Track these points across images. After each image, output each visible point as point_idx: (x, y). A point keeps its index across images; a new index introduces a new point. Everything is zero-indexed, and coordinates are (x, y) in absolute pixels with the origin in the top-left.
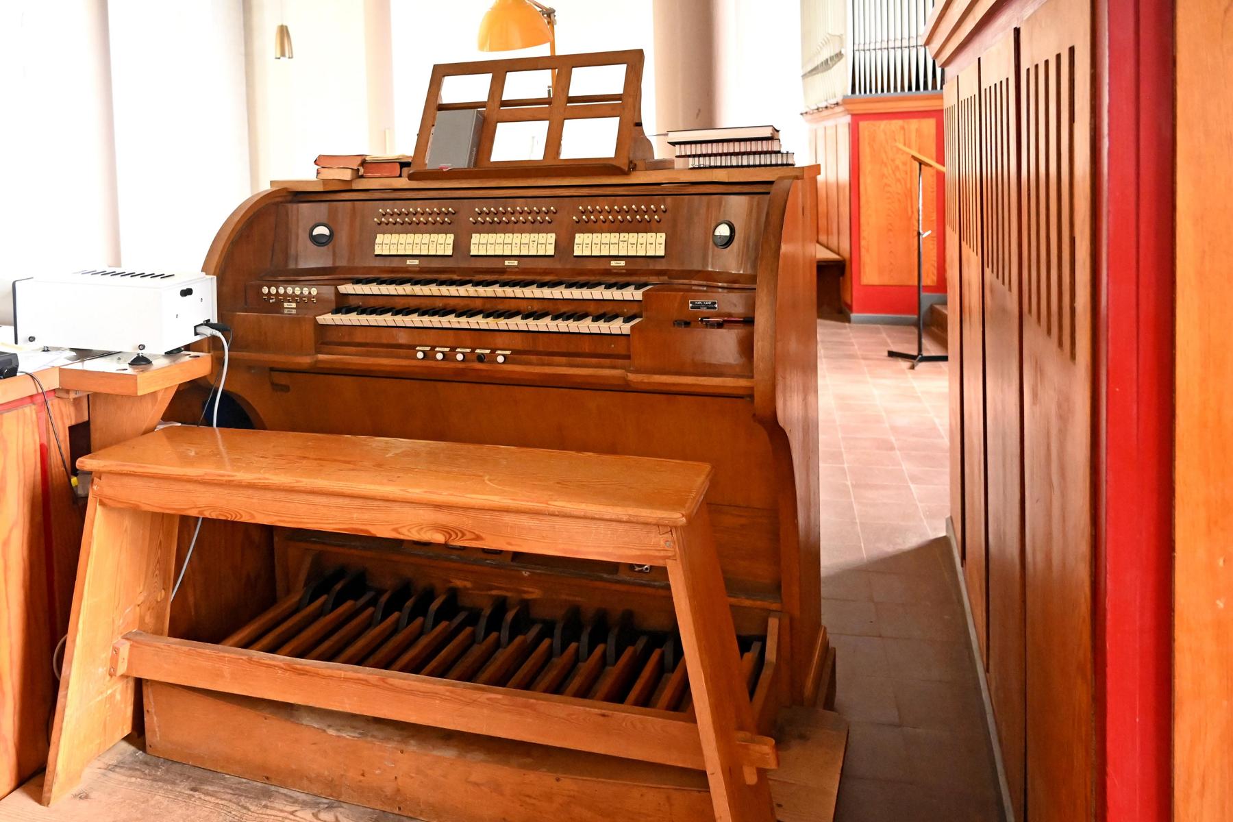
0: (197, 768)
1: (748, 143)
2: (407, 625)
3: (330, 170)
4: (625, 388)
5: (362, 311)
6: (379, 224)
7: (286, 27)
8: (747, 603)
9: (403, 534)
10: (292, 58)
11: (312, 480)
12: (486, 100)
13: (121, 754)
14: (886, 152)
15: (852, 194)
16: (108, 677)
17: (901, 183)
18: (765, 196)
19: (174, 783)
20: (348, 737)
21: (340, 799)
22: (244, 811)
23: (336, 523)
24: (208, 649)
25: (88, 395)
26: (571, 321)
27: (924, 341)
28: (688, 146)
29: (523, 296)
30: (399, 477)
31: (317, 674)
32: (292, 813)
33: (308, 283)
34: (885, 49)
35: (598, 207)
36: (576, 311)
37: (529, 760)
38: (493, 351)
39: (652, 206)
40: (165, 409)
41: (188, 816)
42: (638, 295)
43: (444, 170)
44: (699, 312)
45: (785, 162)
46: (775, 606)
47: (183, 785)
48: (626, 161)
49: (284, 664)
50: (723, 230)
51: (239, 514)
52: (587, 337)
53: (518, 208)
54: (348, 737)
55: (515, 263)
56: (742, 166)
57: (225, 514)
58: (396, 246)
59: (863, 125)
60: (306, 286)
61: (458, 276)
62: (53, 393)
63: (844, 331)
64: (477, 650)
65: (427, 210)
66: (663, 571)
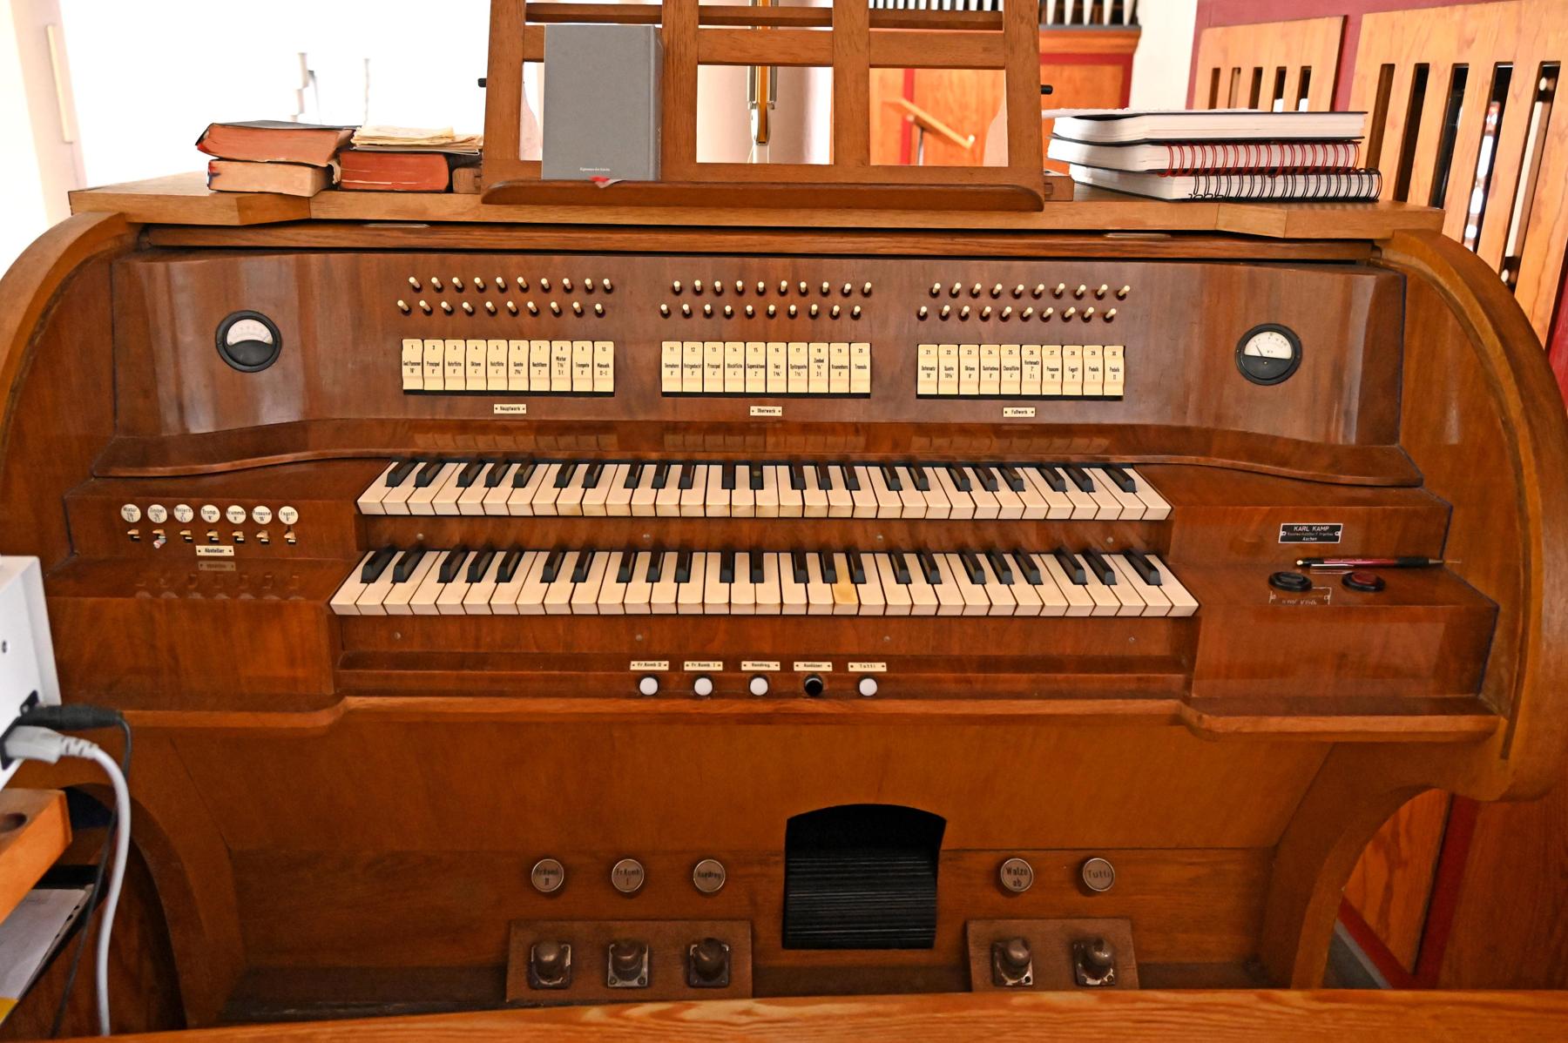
43: (601, 185)
50: (1271, 346)
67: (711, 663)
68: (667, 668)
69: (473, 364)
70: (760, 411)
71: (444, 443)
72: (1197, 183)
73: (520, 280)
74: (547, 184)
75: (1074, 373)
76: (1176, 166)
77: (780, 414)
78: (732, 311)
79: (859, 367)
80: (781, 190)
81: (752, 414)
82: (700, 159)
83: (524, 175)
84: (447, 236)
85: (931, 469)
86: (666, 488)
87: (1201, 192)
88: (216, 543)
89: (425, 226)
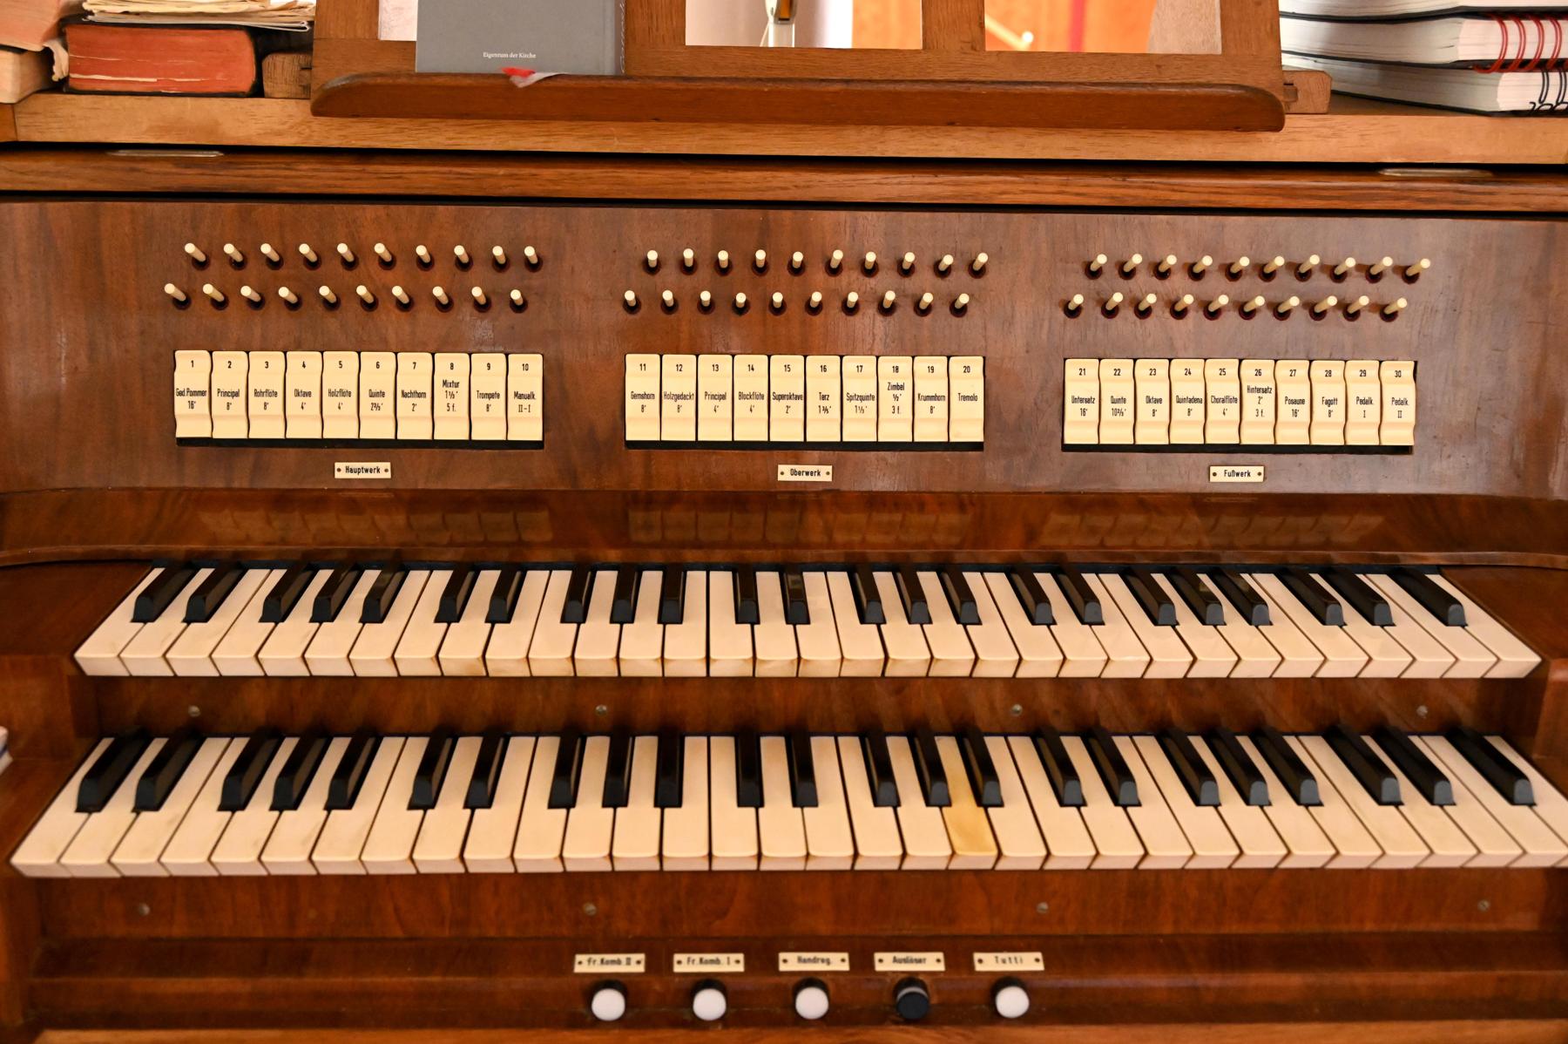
43: (521, 83)
67: (723, 957)
68: (641, 969)
69: (298, 393)
70: (794, 472)
71: (251, 528)
72: (1546, 85)
73: (380, 249)
74: (427, 81)
75: (1332, 407)
76: (1511, 54)
77: (829, 479)
78: (747, 303)
79: (965, 398)
80: (836, 93)
81: (780, 478)
82: (691, 40)
83: (386, 64)
84: (253, 172)
85: (1094, 575)
86: (636, 622)
87: (1551, 99)
89: (213, 155)
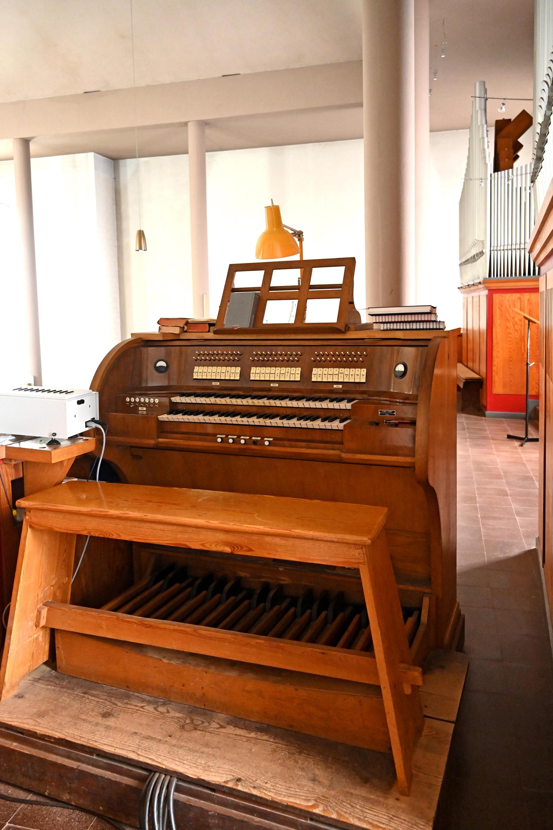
0: (86, 681)
1: (413, 316)
2: (211, 599)
3: (167, 328)
4: (340, 461)
5: (185, 413)
6: (196, 360)
7: (143, 231)
8: (411, 588)
9: (207, 547)
10: (146, 250)
11: (154, 515)
12: (261, 286)
13: (42, 672)
14: (509, 313)
15: (488, 336)
16: (35, 628)
17: (518, 332)
18: (425, 348)
19: (73, 689)
20: (174, 664)
21: (170, 699)
22: (114, 706)
23: (168, 540)
24: (93, 612)
25: (23, 462)
26: (309, 421)
27: (529, 429)
28: (380, 317)
29: (280, 406)
30: (205, 514)
31: (157, 627)
32: (142, 707)
33: (153, 395)
34: (510, 249)
35: (326, 353)
36: (312, 415)
37: (279, 678)
38: (262, 438)
39: (359, 353)
40: (68, 471)
41: (81, 708)
42: (349, 406)
43: (235, 329)
44: (385, 417)
45: (438, 327)
46: (427, 591)
47: (78, 690)
48: (344, 325)
49: (138, 621)
50: (400, 368)
51: (112, 534)
52: (318, 431)
53: (279, 352)
54: (174, 664)
55: (277, 385)
56: (413, 329)
57: (104, 534)
58: (206, 374)
59: (496, 296)
60: (152, 397)
61: (243, 392)
62: (2, 461)
63: (481, 422)
64: (252, 614)
65: (225, 352)
66: (357, 571)
88: (143, 407)
